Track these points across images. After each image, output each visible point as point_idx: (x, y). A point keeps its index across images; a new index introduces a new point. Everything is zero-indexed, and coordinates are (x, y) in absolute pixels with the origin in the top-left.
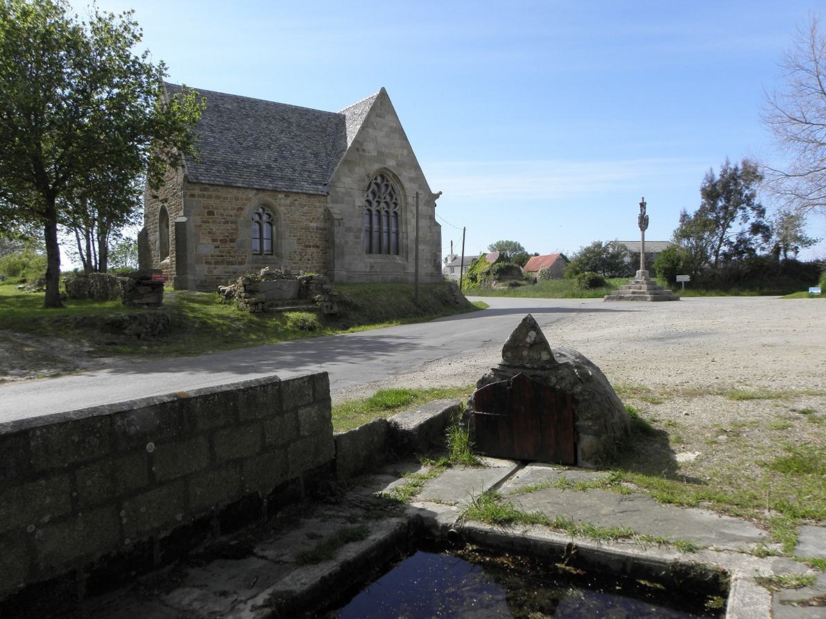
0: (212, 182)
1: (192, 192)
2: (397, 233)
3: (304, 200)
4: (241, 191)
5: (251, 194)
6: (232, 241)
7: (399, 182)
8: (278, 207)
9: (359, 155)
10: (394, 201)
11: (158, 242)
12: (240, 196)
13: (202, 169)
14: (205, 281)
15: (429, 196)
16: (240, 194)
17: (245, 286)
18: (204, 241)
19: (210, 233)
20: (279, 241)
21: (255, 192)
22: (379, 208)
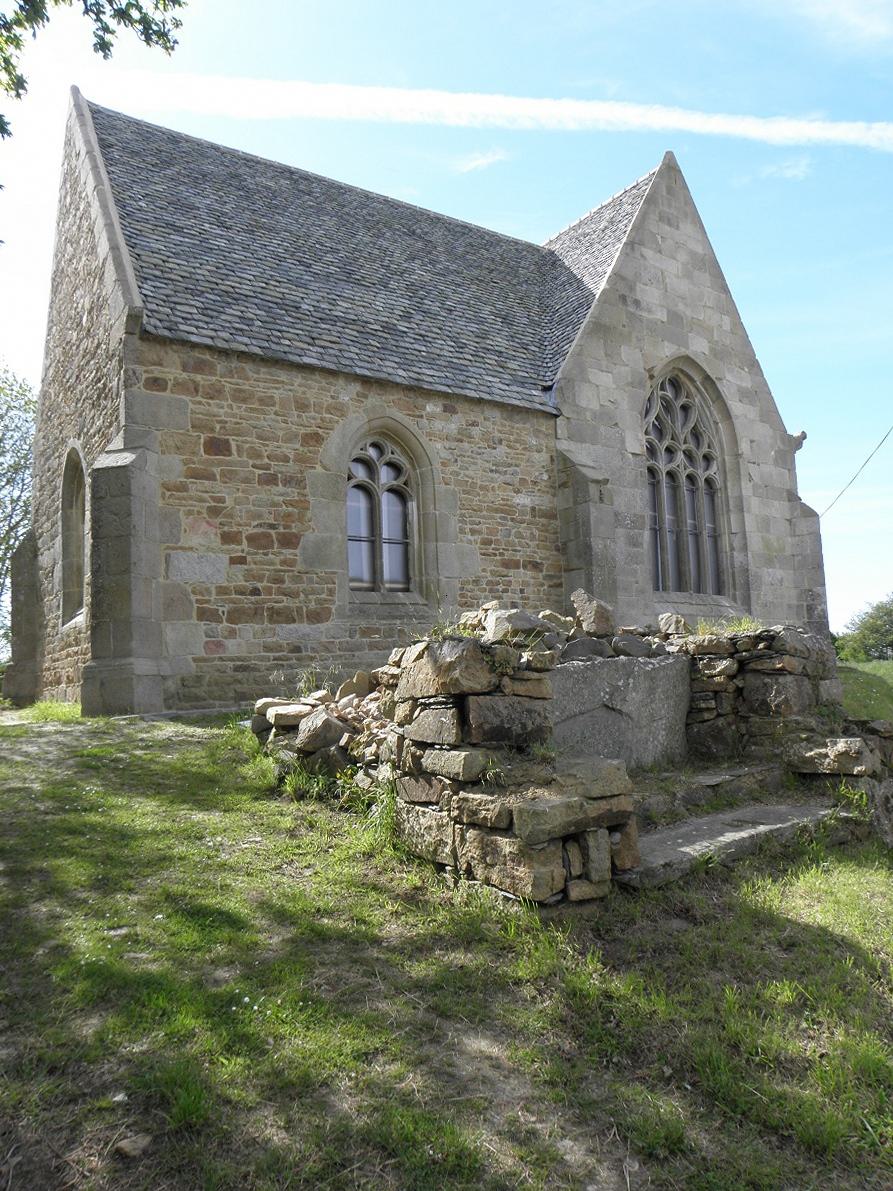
0: (221, 344)
1: (157, 372)
2: (715, 537)
3: (492, 423)
4: (316, 382)
5: (347, 393)
6: (289, 541)
7: (719, 397)
8: (424, 440)
9: (628, 312)
10: (705, 450)
11: (58, 567)
12: (311, 396)
13: (190, 307)
14: (199, 679)
15: (783, 443)
16: (314, 390)
17: (459, 701)
18: (195, 540)
19: (214, 512)
20: (432, 546)
21: (356, 387)
22: (672, 466)
